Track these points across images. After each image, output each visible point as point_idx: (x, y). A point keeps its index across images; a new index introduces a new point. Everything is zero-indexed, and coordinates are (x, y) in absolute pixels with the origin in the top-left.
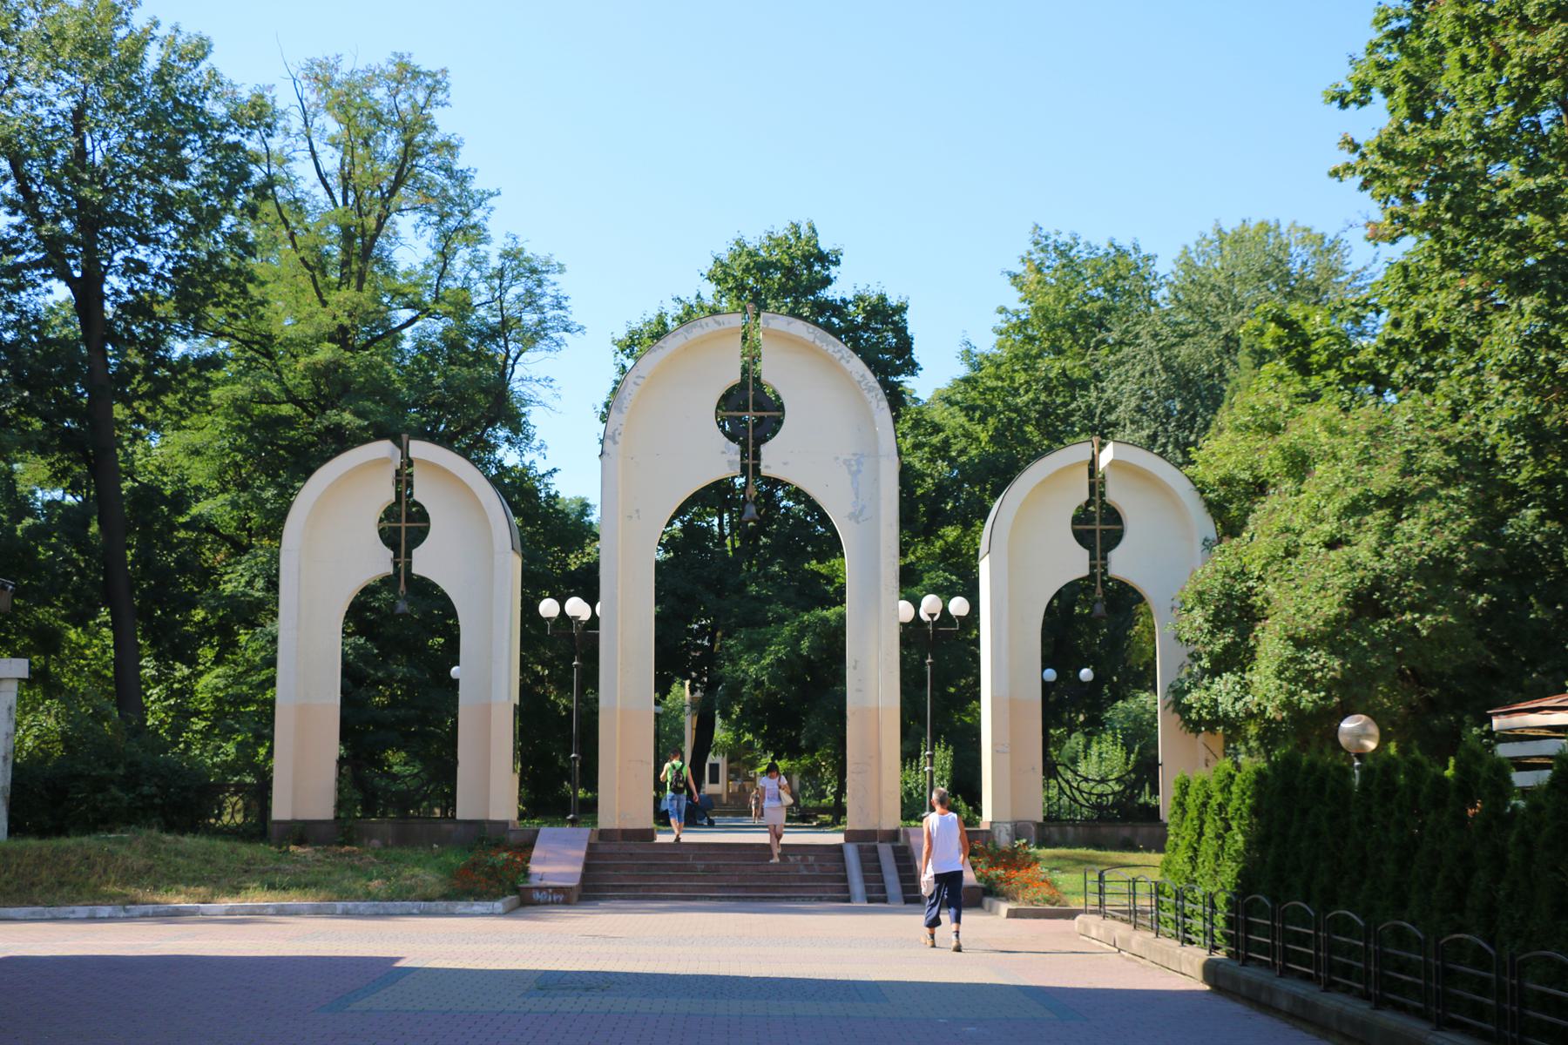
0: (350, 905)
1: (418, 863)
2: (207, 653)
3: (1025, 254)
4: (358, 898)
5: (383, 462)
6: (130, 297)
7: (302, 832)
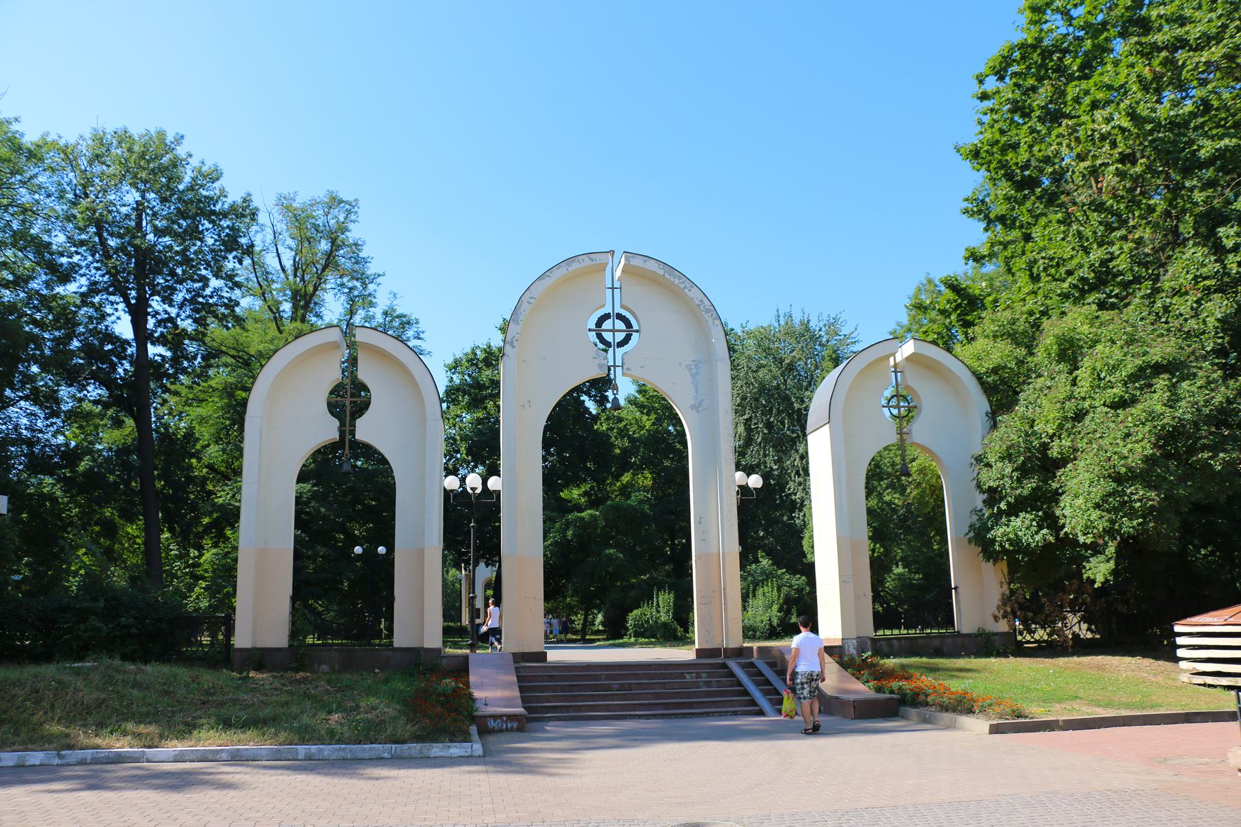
0: (314, 748)
1: (369, 692)
2: (207, 542)
4: (321, 741)
7: (260, 658)
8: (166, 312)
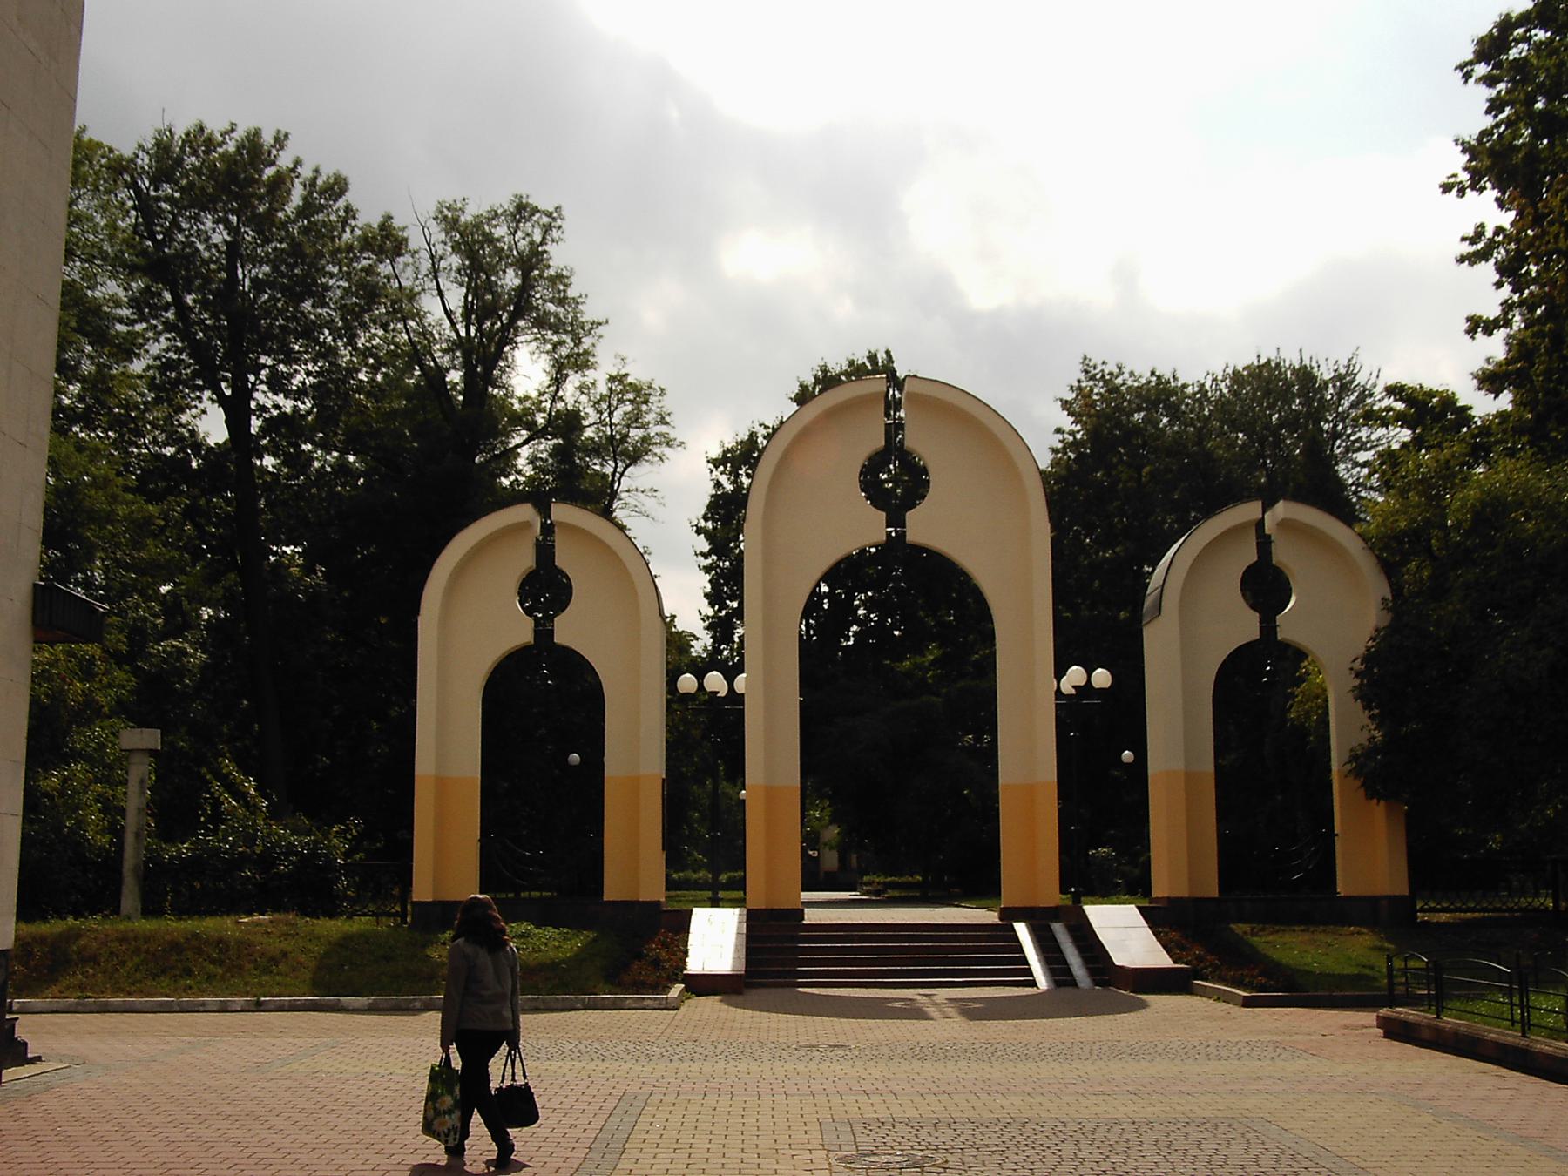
3: (1075, 384)
5: (526, 525)
6: (275, 413)
8: (277, 407)
